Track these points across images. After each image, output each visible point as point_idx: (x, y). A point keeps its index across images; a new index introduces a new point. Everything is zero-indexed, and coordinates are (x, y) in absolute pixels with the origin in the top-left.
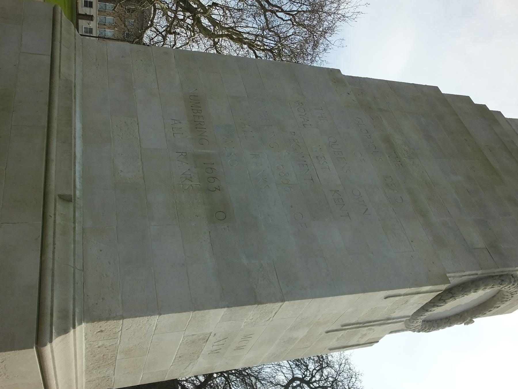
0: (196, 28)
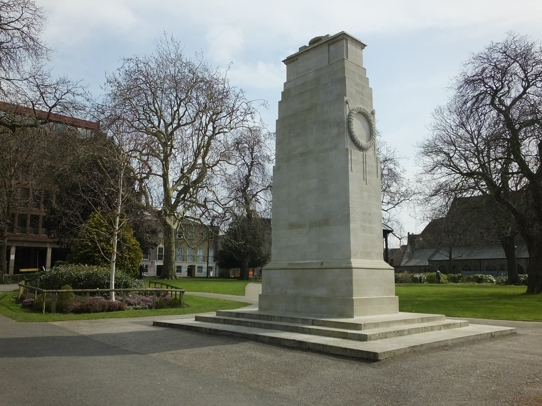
0: (200, 185)
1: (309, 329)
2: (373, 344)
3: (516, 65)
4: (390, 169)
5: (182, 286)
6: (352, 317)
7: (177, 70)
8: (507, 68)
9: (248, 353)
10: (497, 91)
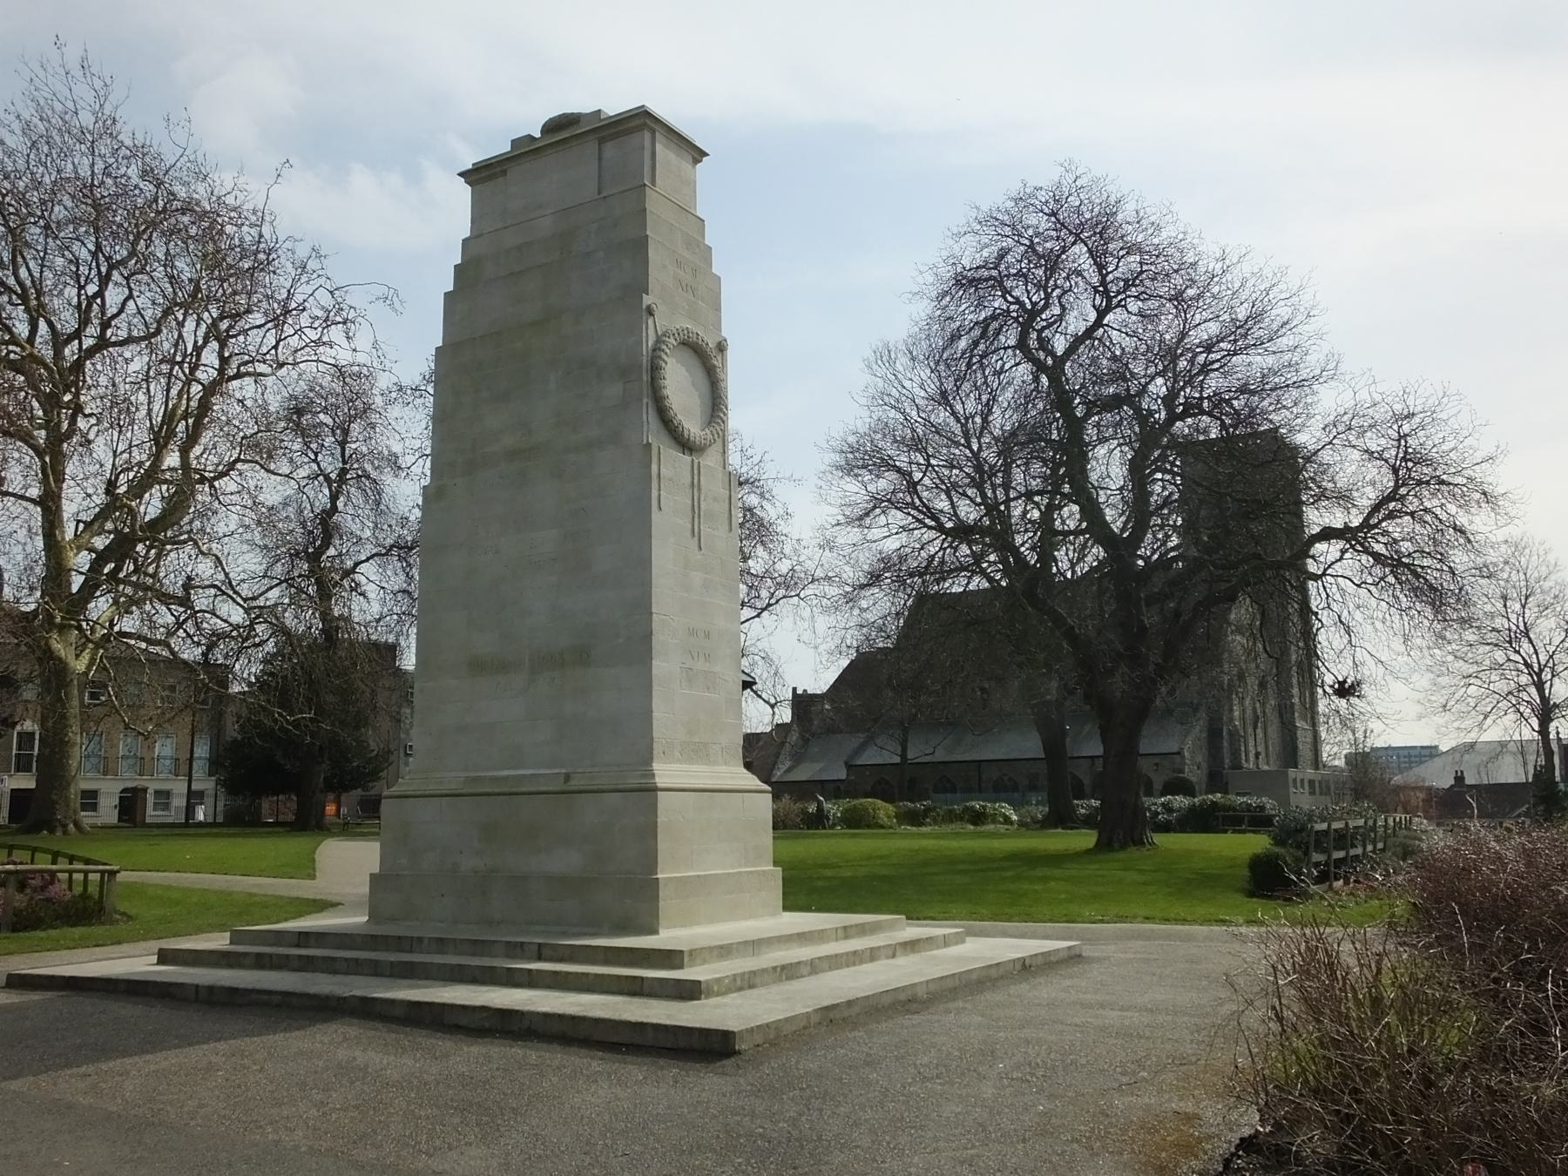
1: (530, 971)
2: (716, 1007)
3: (1079, 249)
4: (750, 510)
5: (108, 853)
6: (655, 932)
7: (100, 166)
8: (1059, 256)
9: (342, 1054)
10: (1034, 313)
